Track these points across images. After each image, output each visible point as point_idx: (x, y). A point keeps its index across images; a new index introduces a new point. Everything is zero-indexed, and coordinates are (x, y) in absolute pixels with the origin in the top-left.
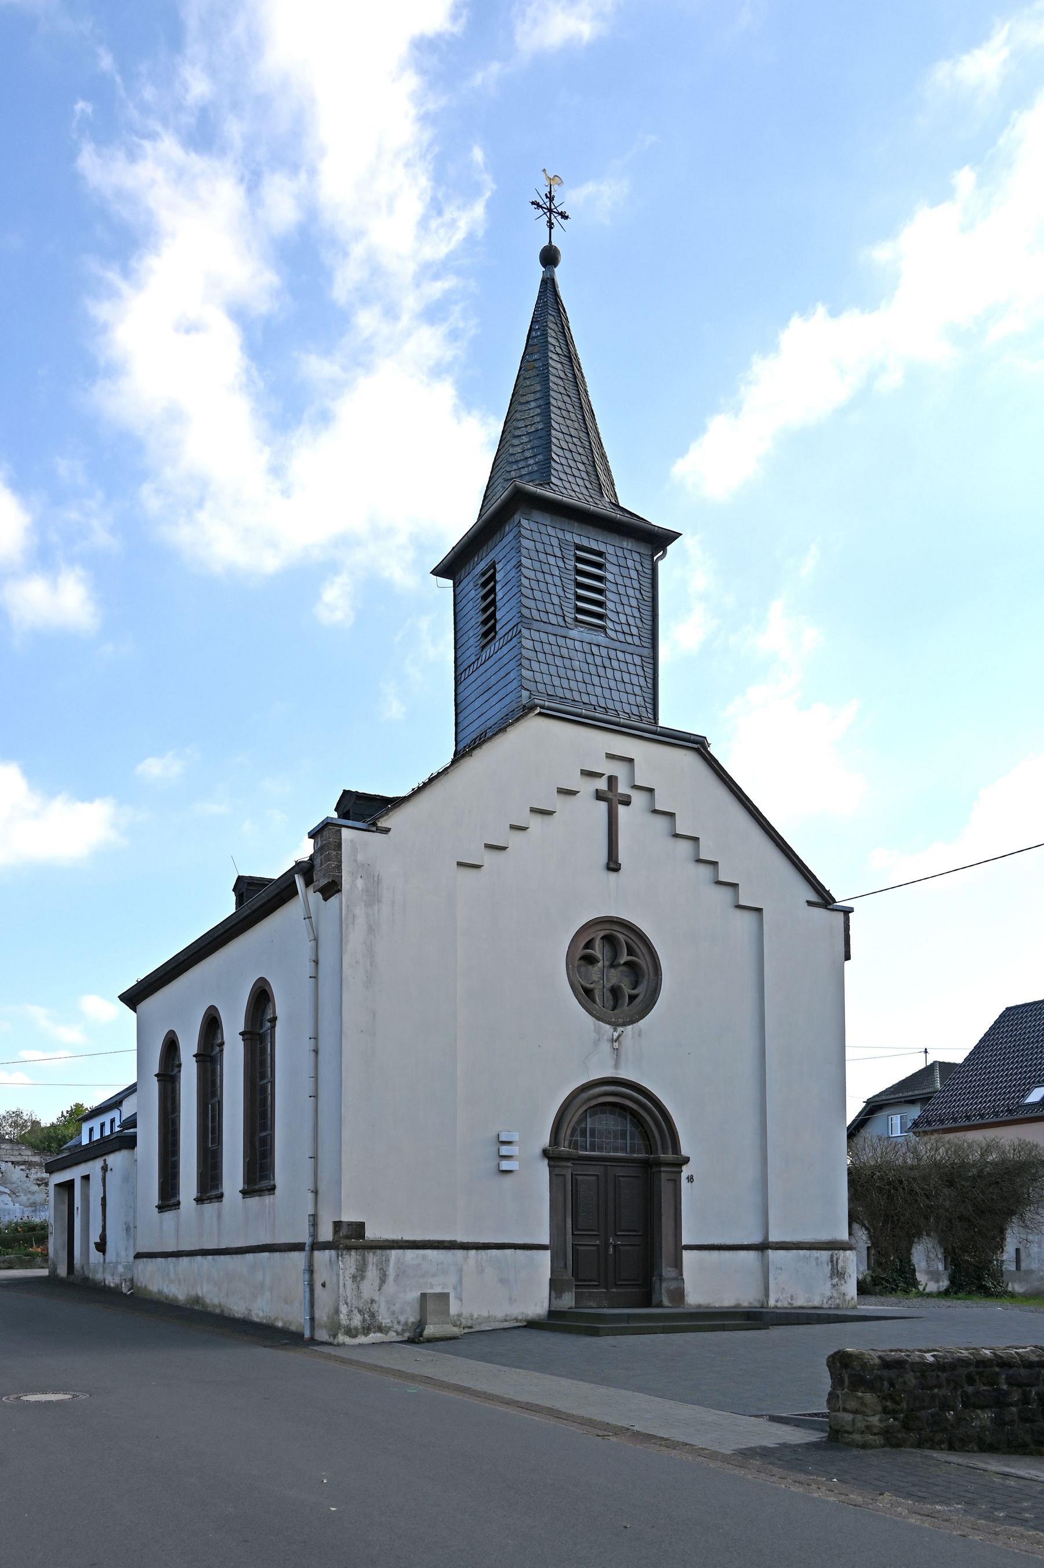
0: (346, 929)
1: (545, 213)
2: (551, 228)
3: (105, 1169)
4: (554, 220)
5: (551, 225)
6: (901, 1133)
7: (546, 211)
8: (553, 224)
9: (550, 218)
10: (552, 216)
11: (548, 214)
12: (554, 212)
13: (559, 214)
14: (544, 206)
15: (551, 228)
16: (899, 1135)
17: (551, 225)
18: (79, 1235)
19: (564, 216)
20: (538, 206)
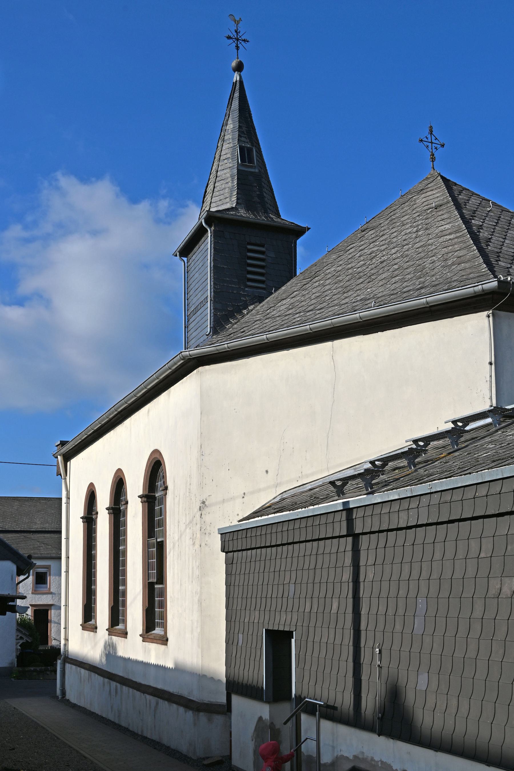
0: (68, 449)
1: (234, 42)
2: (238, 49)
3: (55, 639)
4: (240, 45)
5: (237, 48)
6: (185, 349)
7: (234, 40)
8: (239, 47)
9: (237, 44)
10: (239, 43)
11: (236, 42)
12: (235, 39)
13: (232, 38)
14: (234, 37)
15: (238, 49)
16: (184, 350)
17: (237, 48)
18: (59, 679)
19: (229, 38)
20: (244, 41)
